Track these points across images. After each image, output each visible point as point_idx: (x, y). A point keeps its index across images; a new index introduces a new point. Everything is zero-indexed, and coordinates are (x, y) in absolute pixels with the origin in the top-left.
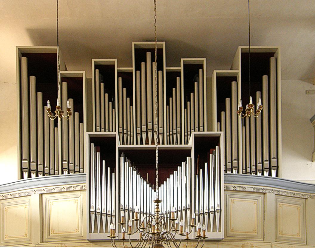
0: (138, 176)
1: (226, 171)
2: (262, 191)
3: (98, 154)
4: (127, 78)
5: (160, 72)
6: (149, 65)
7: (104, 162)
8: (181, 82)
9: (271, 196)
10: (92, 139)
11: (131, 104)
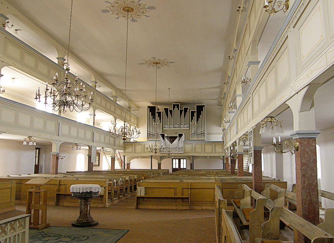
4: (171, 111)
8: (183, 112)
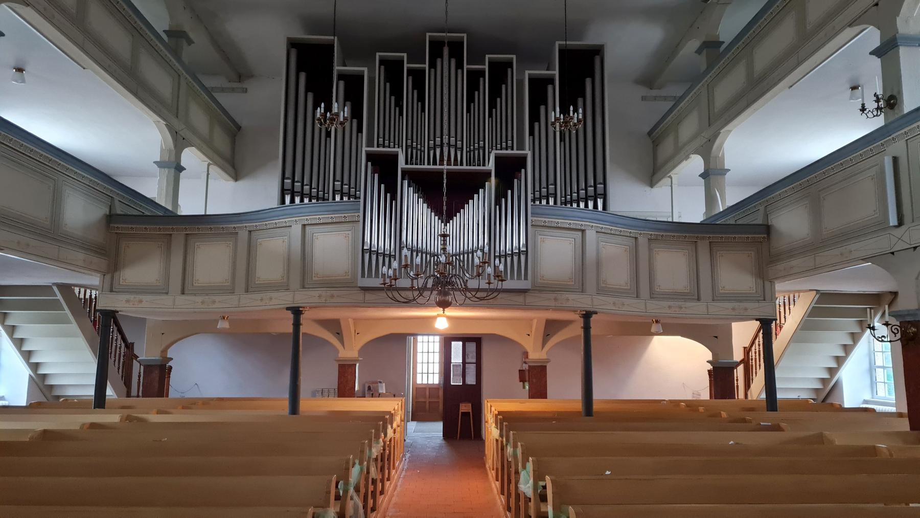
0: (425, 205)
1: (534, 201)
2: (579, 227)
3: (376, 176)
4: (418, 77)
5: (460, 71)
6: (446, 62)
7: (383, 186)
8: (485, 84)
9: (591, 235)
10: (370, 157)
11: (423, 110)
